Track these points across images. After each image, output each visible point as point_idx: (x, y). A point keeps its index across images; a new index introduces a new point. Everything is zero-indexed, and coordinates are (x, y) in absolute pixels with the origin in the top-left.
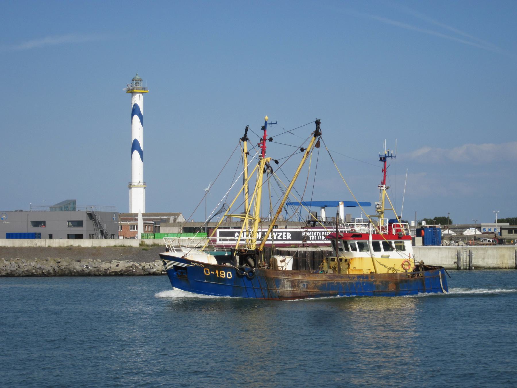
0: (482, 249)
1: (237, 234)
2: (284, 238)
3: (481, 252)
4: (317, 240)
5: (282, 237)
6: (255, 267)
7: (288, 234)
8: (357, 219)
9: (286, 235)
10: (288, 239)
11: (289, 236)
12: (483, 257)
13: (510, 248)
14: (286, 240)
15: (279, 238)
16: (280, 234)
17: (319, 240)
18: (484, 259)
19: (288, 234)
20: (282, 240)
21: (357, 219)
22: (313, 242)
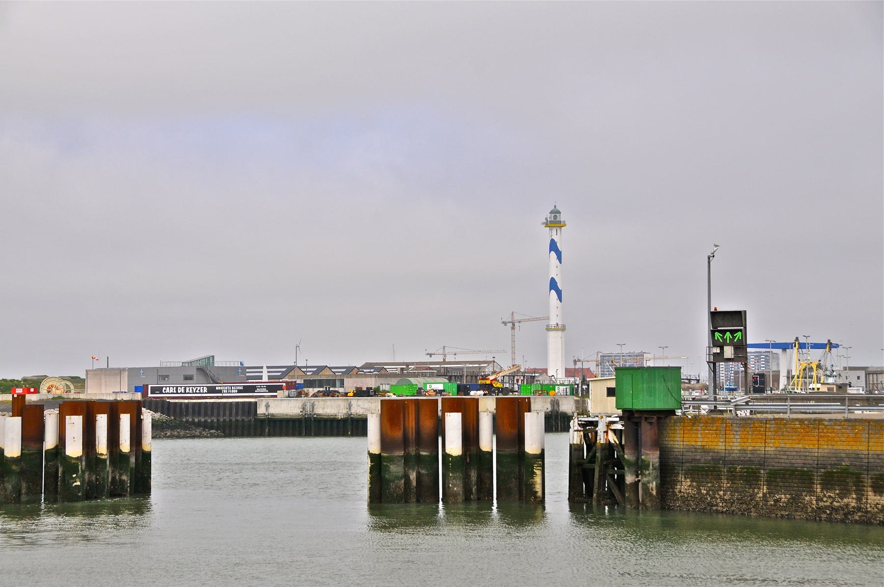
0: (322, 400)
1: (164, 389)
2: (201, 392)
3: (321, 403)
4: (228, 393)
5: (200, 390)
6: (779, 533)
7: (205, 388)
8: (151, 387)
9: (203, 389)
10: (171, 392)
11: (205, 391)
12: (323, 407)
13: (345, 399)
14: (203, 393)
15: (197, 391)
16: (199, 388)
17: (230, 393)
18: (324, 408)
19: (205, 388)
20: (200, 393)
21: (151, 387)
22: (224, 395)
